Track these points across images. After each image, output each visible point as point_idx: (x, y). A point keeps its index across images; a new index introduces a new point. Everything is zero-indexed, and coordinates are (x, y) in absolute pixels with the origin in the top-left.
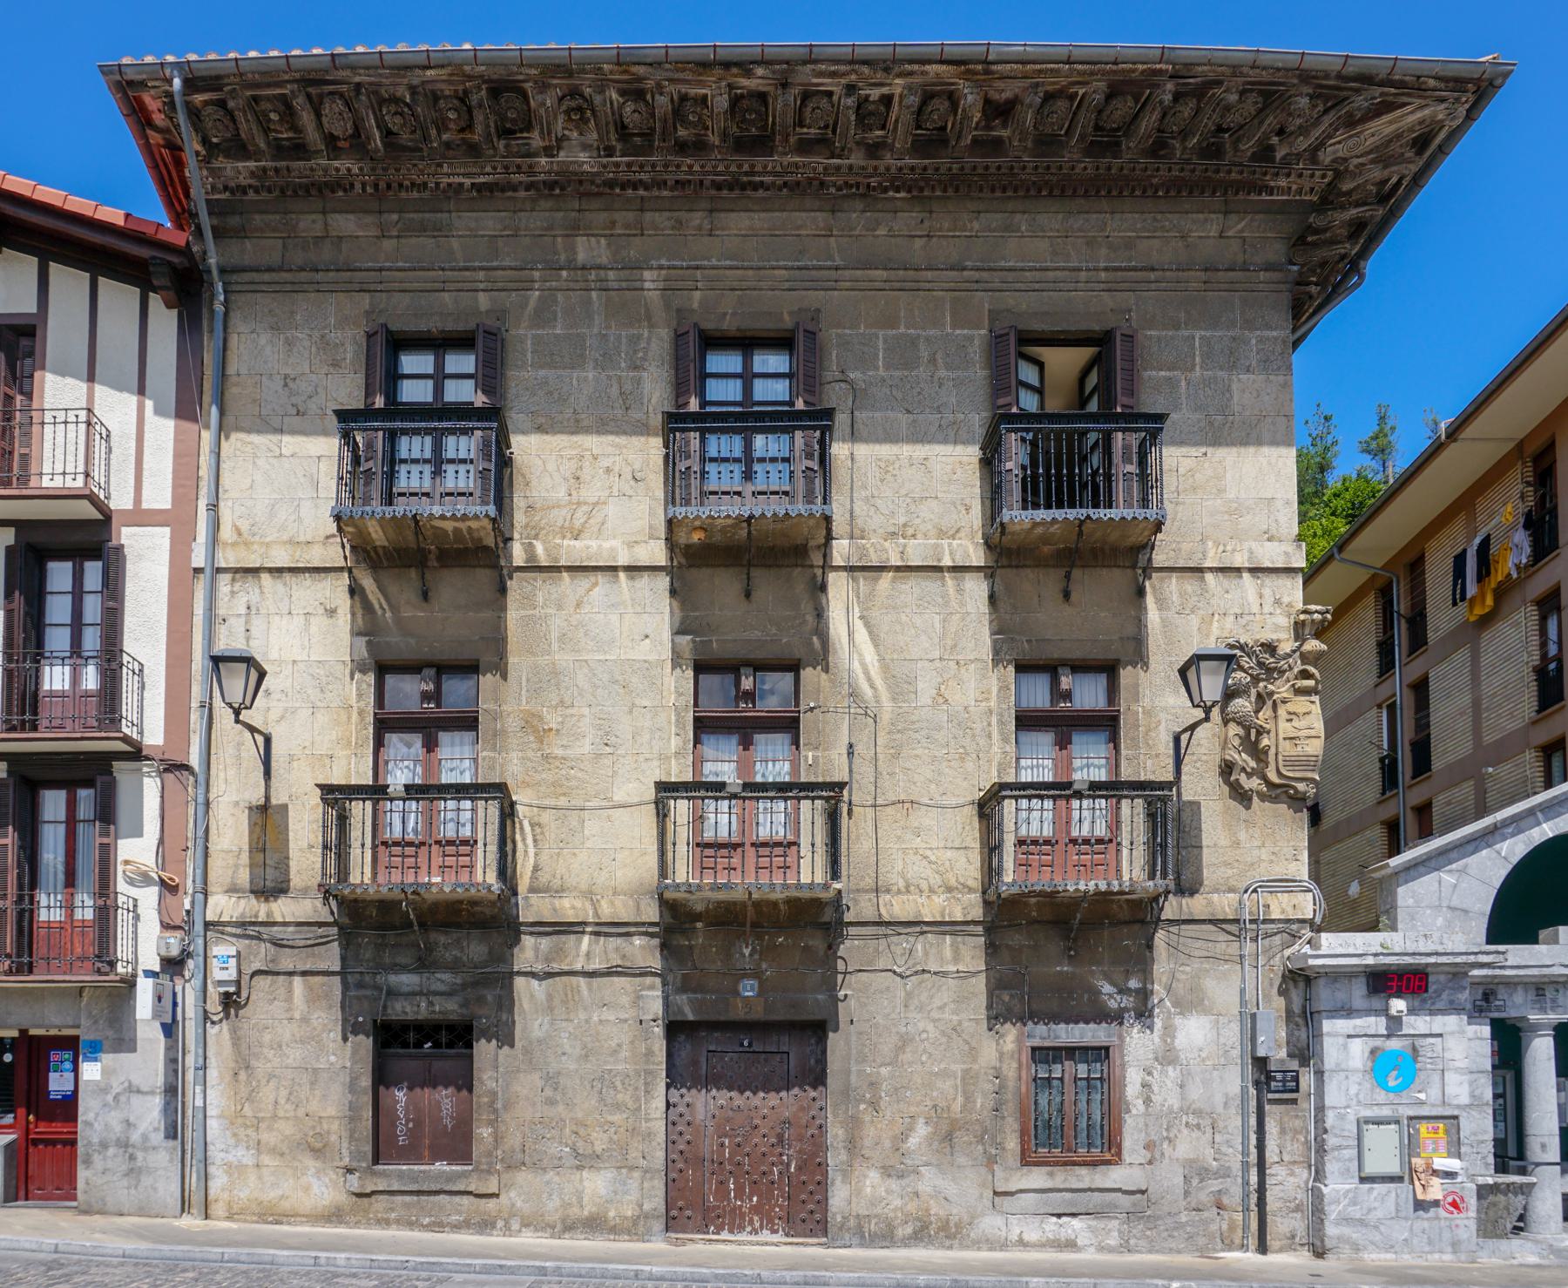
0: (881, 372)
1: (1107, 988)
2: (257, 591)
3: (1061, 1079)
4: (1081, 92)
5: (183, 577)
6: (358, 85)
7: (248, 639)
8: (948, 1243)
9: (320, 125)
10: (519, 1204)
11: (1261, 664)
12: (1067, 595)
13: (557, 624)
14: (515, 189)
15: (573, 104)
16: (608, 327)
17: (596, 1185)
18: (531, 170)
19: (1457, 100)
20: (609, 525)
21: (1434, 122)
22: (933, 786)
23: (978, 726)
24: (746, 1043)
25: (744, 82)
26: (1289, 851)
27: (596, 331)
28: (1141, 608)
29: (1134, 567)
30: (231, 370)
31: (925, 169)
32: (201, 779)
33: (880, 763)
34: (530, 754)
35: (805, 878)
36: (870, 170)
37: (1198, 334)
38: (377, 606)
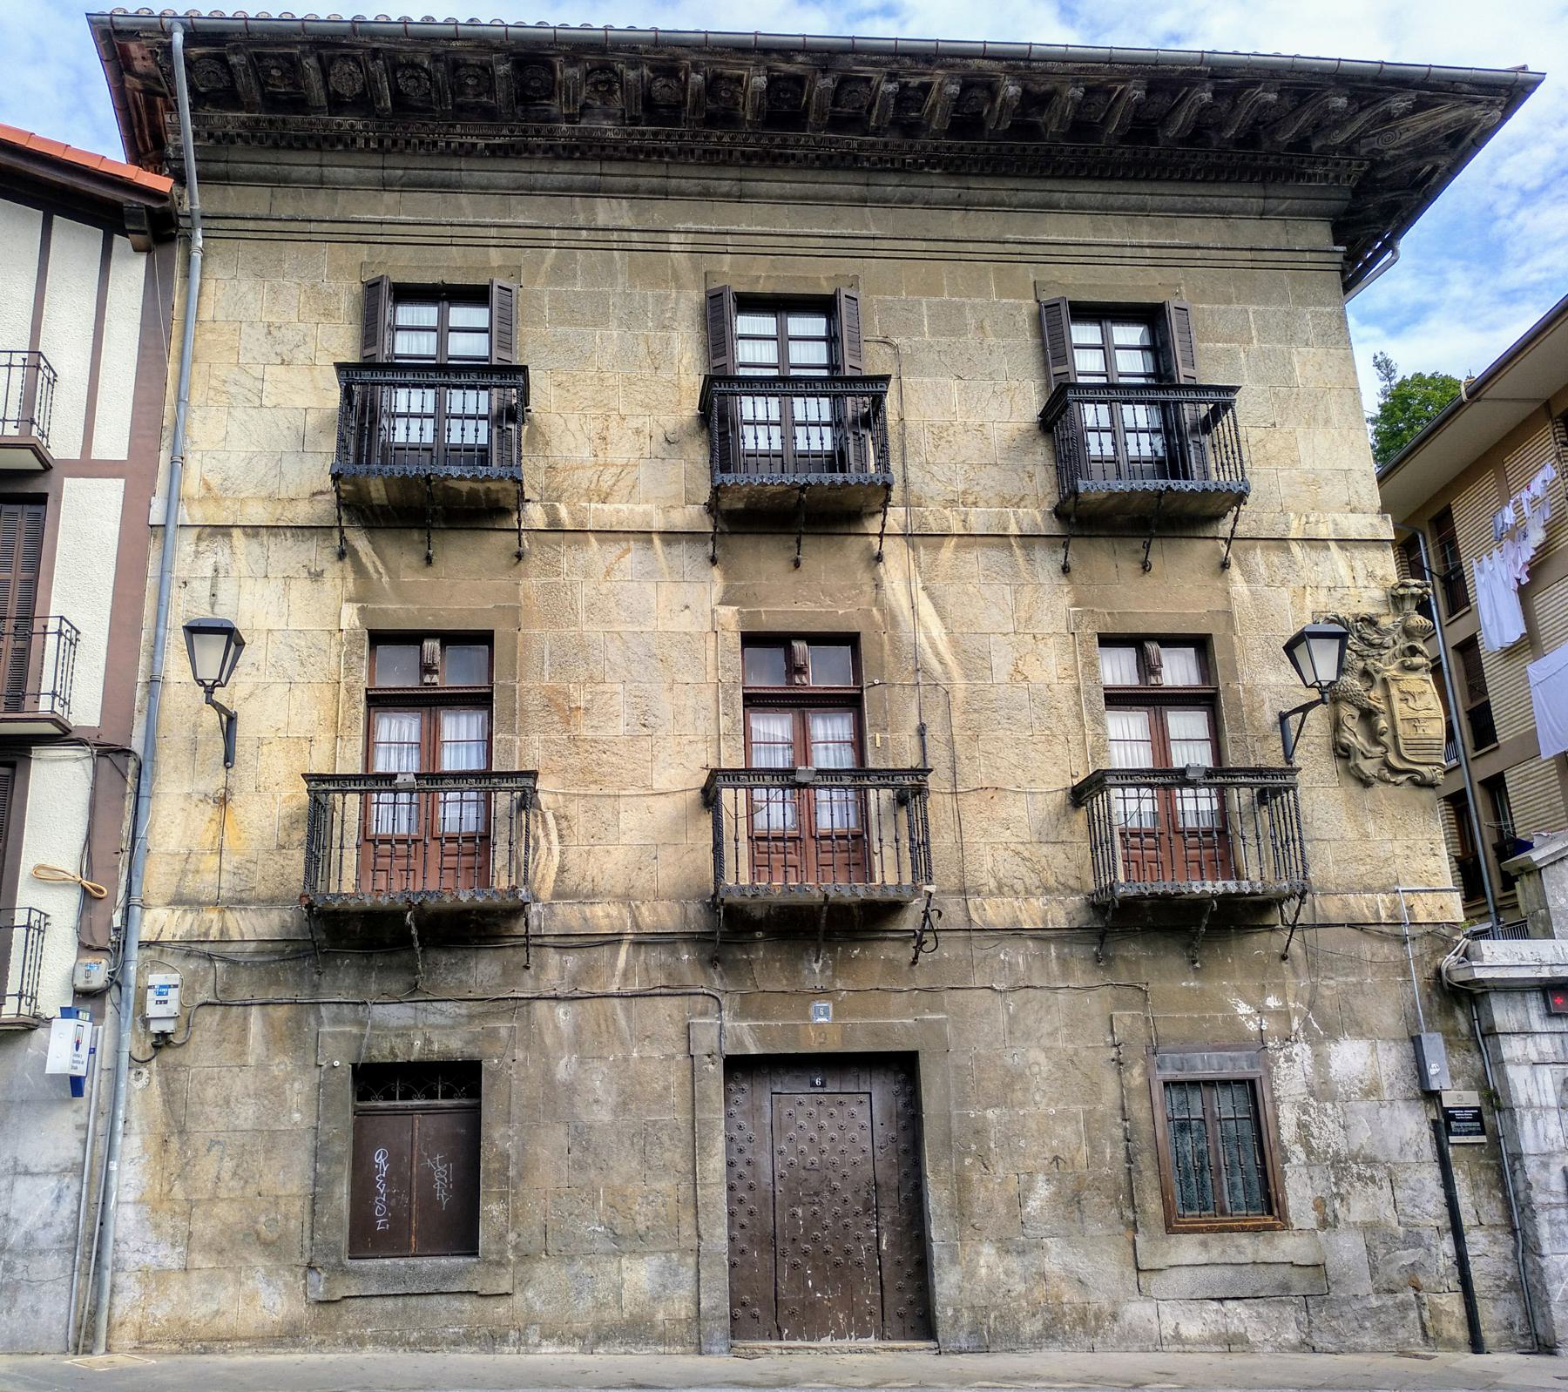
0: (927, 338)
1: (1243, 1009)
2: (227, 551)
3: (1203, 1121)
4: (1120, 88)
5: (142, 539)
6: (377, 50)
7: (212, 606)
8: (1087, 1342)
9: (326, 83)
10: (538, 1306)
13: (584, 592)
15: (602, 77)
16: (633, 286)
17: (639, 1275)
18: (551, 134)
19: (1491, 102)
20: (641, 488)
21: (1469, 120)
22: (1019, 772)
24: (818, 1082)
25: (784, 67)
26: (1423, 845)
27: (619, 289)
31: (962, 148)
33: (957, 746)
34: (554, 736)
36: (906, 147)
37: (1251, 308)
38: (371, 570)
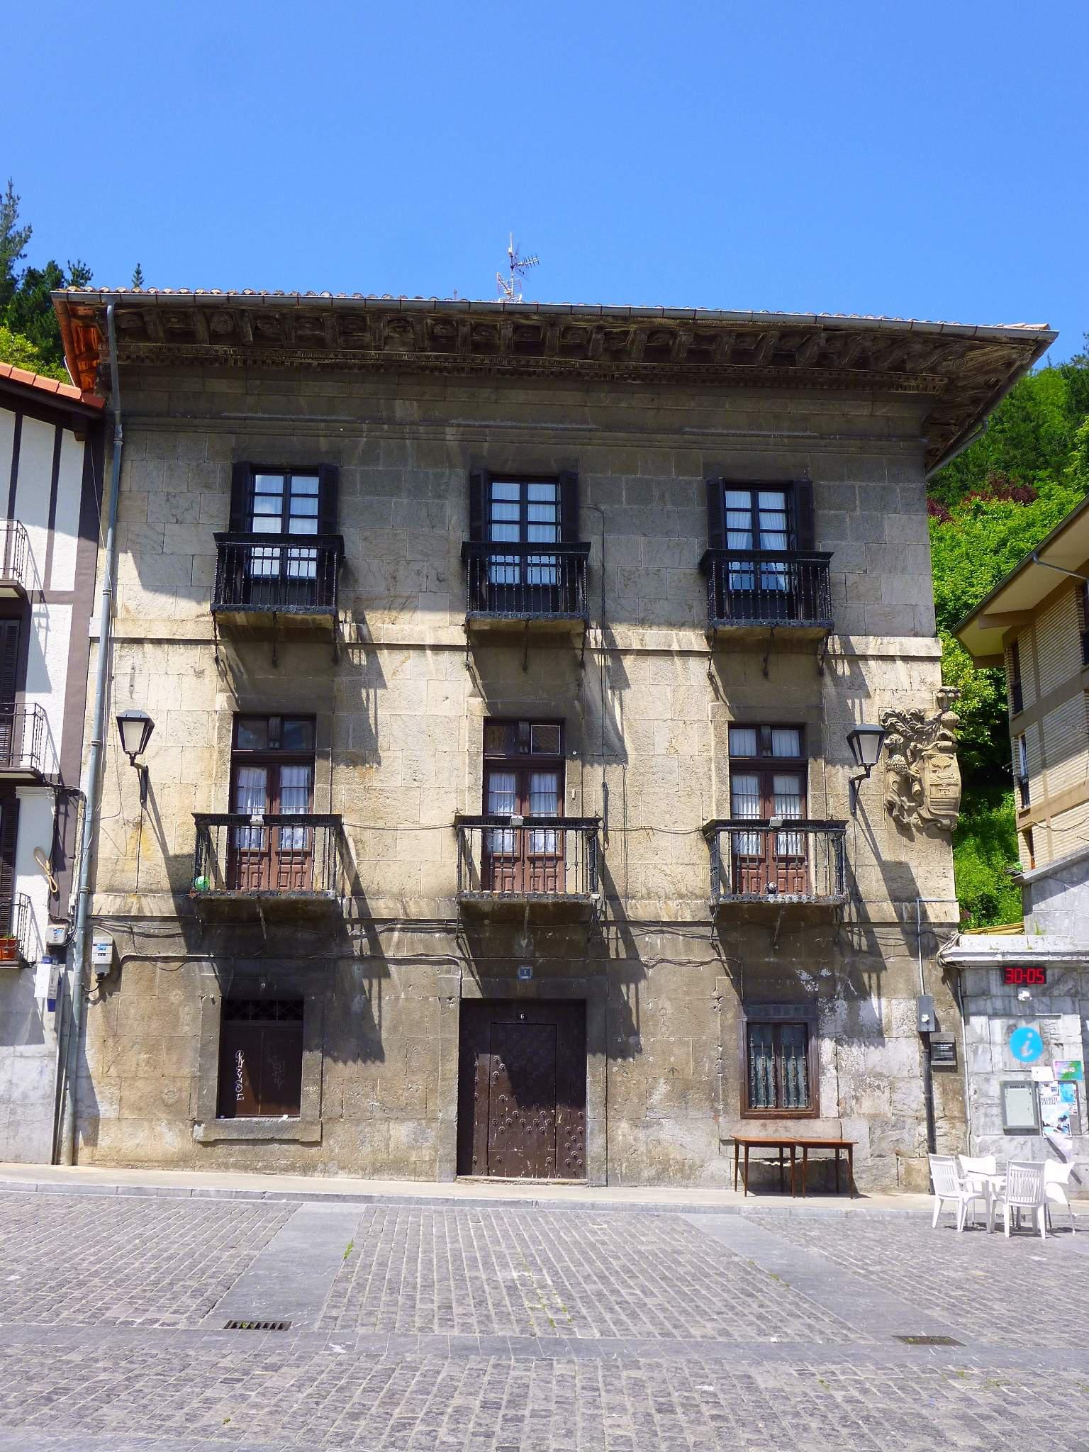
1: (805, 976)
2: (140, 656)
5: (81, 643)
11: (912, 729)
12: (766, 674)
14: (350, 368)
17: (401, 1132)
18: (363, 357)
19: (1023, 349)
23: (701, 771)
26: (939, 870)
27: (409, 468)
28: (821, 685)
29: (816, 654)
30: (125, 487)
32: (89, 802)
34: (354, 786)
35: (571, 889)
